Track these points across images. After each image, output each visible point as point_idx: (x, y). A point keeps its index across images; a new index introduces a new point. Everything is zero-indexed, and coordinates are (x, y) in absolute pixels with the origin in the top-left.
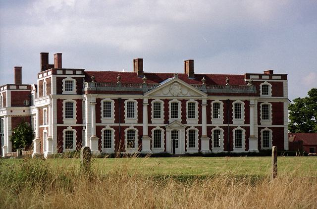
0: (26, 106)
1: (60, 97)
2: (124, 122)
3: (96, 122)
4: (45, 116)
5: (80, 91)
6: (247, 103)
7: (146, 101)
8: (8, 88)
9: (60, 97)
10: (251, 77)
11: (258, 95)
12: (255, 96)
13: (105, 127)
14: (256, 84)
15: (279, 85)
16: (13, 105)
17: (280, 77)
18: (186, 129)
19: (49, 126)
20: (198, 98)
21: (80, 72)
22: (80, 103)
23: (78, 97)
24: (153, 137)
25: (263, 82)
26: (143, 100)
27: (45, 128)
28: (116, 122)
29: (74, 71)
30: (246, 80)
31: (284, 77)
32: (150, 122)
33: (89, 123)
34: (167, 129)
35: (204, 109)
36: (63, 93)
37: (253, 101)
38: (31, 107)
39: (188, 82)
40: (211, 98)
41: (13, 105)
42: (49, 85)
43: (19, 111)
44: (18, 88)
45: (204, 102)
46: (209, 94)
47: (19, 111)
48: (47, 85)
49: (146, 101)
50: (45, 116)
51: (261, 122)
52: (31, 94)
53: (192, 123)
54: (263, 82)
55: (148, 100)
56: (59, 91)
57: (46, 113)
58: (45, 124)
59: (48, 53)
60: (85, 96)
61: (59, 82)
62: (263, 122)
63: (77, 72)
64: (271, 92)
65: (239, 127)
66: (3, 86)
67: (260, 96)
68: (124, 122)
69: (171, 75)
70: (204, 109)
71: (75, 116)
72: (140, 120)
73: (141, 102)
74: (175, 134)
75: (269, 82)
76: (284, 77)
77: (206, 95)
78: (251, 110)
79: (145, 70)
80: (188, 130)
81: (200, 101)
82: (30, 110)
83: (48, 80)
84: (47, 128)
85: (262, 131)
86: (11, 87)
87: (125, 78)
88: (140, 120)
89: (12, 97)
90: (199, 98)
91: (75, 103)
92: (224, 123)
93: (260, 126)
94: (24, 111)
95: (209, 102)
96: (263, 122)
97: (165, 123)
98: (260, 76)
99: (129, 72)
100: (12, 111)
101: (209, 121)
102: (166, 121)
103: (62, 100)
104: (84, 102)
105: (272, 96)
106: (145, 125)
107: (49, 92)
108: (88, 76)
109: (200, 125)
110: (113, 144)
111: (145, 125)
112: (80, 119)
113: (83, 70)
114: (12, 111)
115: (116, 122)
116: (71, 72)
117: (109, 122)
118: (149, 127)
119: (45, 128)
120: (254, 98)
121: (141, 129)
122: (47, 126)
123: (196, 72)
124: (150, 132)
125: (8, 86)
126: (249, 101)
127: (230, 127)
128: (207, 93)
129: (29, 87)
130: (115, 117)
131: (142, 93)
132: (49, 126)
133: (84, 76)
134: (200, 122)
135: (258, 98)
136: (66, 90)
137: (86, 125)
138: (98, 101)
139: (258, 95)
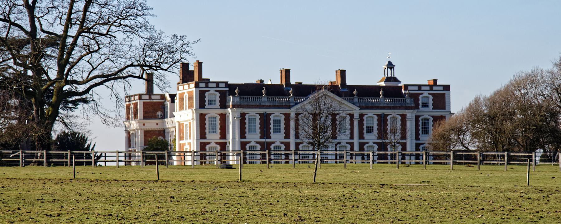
0: (160, 119)
1: (203, 111)
2: (270, 138)
3: (201, 138)
4: (186, 130)
5: (224, 105)
6: (404, 117)
7: (293, 115)
8: (140, 98)
9: (203, 111)
10: (410, 88)
11: (416, 107)
12: (412, 109)
13: (249, 142)
14: (415, 97)
15: (440, 95)
16: (145, 117)
18: (336, 145)
19: (191, 141)
20: (349, 112)
21: (223, 85)
22: (223, 118)
23: (222, 111)
25: (422, 94)
26: (290, 114)
27: (187, 144)
28: (261, 138)
29: (218, 84)
30: (403, 92)
33: (234, 139)
35: (356, 123)
36: (206, 107)
37: (410, 115)
38: (166, 120)
39: (339, 94)
40: (364, 112)
41: (145, 117)
42: (191, 98)
43: (152, 125)
44: (150, 98)
45: (356, 116)
46: (361, 108)
47: (152, 125)
48: (189, 98)
49: (293, 115)
50: (186, 130)
51: (420, 137)
52: (164, 105)
54: (422, 94)
55: (296, 114)
56: (202, 104)
57: (188, 129)
58: (187, 139)
60: (229, 110)
61: (202, 96)
63: (221, 85)
64: (431, 105)
66: (135, 95)
67: (419, 109)
68: (270, 138)
69: (320, 87)
70: (356, 123)
71: (219, 131)
72: (287, 136)
73: (287, 116)
75: (429, 94)
76: (447, 88)
77: (358, 109)
78: (408, 124)
79: (293, 82)
80: (338, 145)
81: (352, 116)
82: (164, 123)
83: (190, 93)
84: (189, 144)
86: (143, 97)
87: (274, 90)
88: (287, 136)
89: (144, 108)
90: (351, 112)
91: (218, 117)
93: (418, 142)
94: (157, 124)
95: (361, 116)
97: (285, 138)
98: (420, 86)
99: (274, 83)
100: (144, 125)
101: (361, 136)
103: (205, 115)
104: (228, 116)
105: (433, 109)
107: (191, 106)
108: (231, 88)
109: (351, 141)
112: (224, 135)
113: (226, 83)
114: (144, 125)
115: (261, 138)
116: (214, 85)
117: (254, 137)
118: (296, 143)
119: (187, 144)
120: (411, 111)
121: (287, 145)
122: (189, 141)
123: (349, 82)
125: (140, 96)
126: (406, 115)
127: (264, 138)
128: (359, 107)
129: (163, 97)
130: (285, 133)
131: (289, 107)
132: (191, 141)
133: (227, 89)
134: (352, 138)
135: (415, 111)
136: (209, 104)
137: (231, 141)
138: (243, 115)
139: (416, 107)
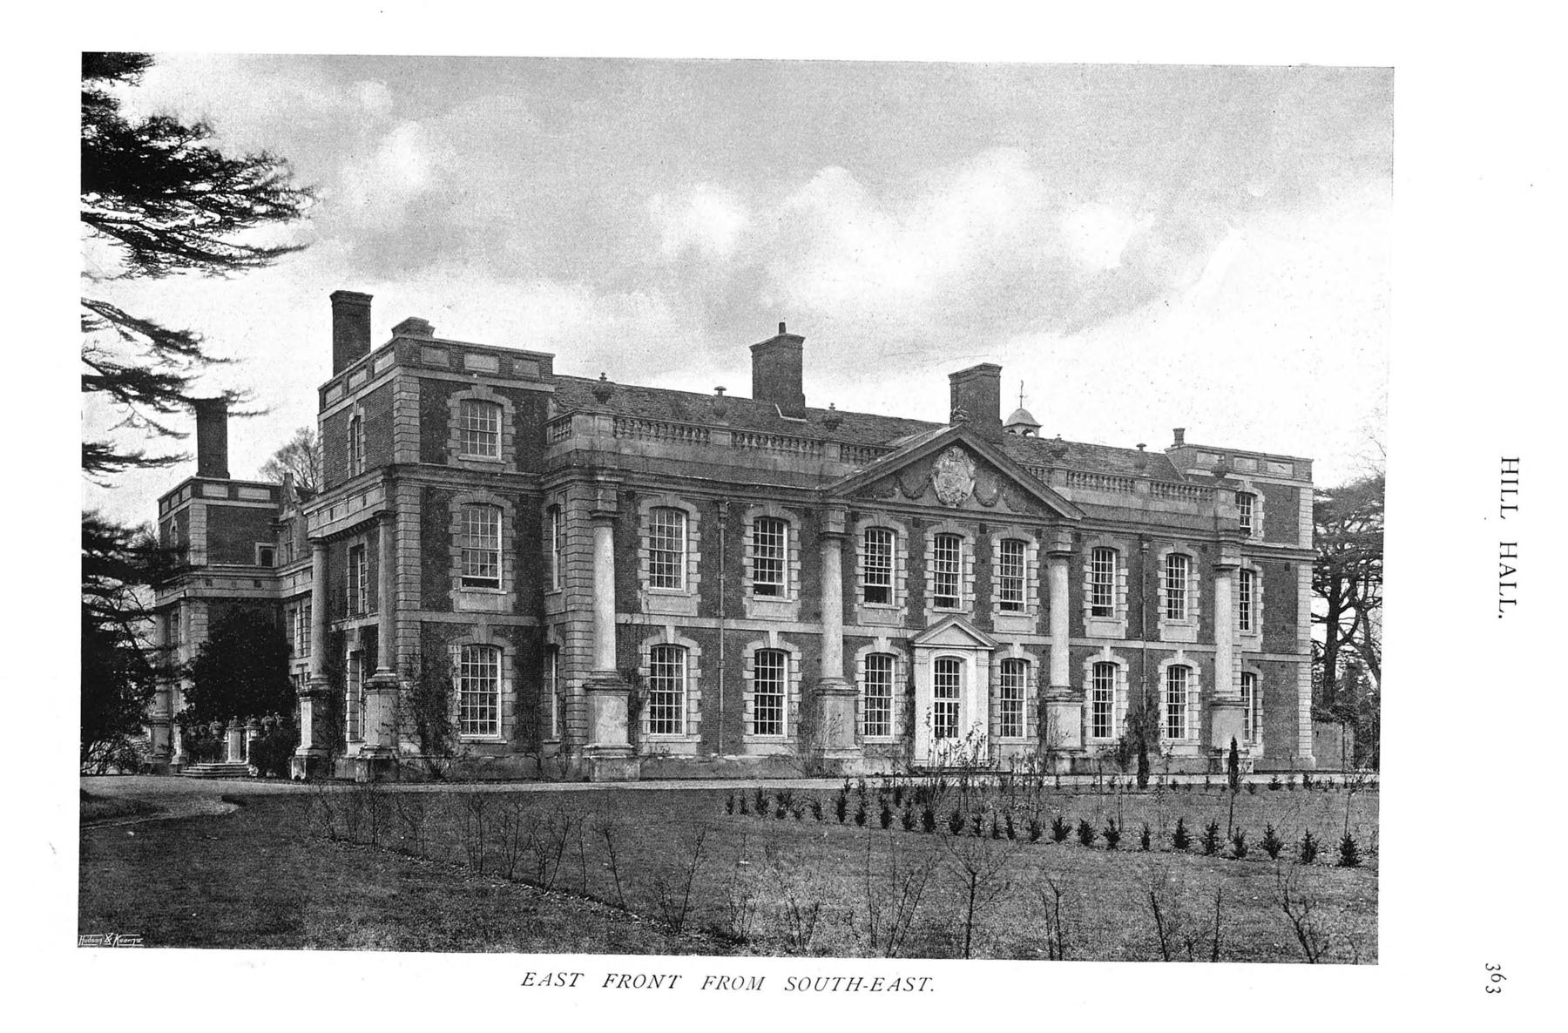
17: (265, 494)
24: (1090, 695)
31: (1370, 495)
32: (848, 617)
34: (917, 652)
53: (1015, 629)
59: (84, 54)
62: (1095, 627)
65: (1107, 648)
74: (948, 670)
85: (862, 654)
92: (700, 615)
93: (852, 631)
96: (1095, 627)
101: (1076, 629)
102: (916, 620)
106: (834, 631)
109: (1041, 640)
110: (499, 729)
111: (834, 631)
124: (849, 671)
134: (1044, 628)
